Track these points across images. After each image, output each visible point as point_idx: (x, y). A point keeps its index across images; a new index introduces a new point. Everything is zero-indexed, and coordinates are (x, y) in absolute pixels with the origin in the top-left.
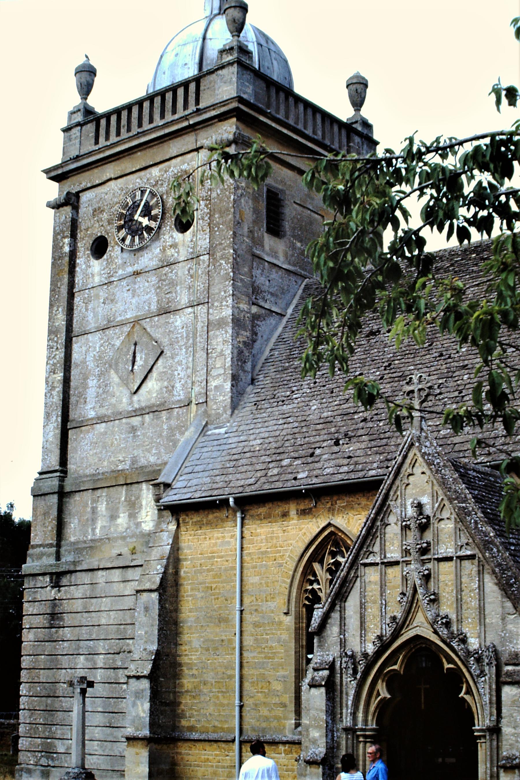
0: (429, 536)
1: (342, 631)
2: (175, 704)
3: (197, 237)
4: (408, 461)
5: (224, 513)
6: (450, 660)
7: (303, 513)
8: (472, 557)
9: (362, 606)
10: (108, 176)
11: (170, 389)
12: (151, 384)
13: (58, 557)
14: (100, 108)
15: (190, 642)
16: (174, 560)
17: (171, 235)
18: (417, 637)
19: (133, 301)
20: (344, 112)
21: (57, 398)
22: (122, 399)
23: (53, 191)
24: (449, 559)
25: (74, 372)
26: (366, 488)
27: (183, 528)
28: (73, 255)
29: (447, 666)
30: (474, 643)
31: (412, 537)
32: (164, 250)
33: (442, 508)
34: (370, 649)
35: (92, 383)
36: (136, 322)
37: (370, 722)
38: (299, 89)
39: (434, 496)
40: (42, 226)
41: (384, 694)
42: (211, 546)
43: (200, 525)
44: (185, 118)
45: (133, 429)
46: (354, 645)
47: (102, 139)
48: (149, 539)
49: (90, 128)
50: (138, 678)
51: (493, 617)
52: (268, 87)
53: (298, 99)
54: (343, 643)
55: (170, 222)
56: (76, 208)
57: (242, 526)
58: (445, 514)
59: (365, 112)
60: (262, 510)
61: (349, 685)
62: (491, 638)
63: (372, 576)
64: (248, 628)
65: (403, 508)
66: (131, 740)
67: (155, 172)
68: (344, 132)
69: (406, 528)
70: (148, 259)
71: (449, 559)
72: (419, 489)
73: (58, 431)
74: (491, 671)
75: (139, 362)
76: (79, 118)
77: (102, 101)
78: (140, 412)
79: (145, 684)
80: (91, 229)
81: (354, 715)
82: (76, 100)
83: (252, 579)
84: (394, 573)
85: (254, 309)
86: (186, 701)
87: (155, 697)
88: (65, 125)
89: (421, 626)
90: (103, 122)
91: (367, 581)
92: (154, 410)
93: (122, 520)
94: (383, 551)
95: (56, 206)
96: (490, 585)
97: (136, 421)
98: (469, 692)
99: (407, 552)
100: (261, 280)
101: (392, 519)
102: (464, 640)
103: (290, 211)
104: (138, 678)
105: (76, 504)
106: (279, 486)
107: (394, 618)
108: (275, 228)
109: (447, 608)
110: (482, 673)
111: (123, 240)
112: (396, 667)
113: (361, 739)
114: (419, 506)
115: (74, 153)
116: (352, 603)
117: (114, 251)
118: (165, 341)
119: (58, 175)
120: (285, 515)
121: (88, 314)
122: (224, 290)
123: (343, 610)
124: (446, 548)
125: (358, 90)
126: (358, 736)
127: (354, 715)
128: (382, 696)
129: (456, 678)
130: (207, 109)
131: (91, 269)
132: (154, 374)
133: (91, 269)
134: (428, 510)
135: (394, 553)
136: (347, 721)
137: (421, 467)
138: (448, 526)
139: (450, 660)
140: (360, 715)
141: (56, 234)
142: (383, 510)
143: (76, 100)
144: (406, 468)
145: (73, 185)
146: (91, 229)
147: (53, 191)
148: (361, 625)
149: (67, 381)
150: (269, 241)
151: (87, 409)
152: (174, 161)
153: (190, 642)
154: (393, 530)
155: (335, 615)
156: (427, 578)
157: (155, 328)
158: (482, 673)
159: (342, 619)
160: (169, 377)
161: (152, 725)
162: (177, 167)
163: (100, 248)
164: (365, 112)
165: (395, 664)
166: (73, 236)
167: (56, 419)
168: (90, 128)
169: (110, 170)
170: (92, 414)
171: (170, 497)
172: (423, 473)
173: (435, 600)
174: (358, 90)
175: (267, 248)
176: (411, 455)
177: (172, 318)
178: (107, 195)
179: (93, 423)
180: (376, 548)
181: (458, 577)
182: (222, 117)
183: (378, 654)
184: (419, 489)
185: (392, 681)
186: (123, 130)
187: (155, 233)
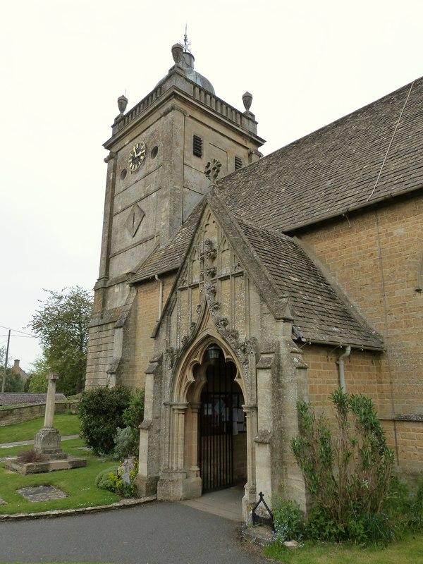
1: (169, 336)
4: (205, 215)
5: (154, 285)
8: (241, 274)
15: (300, 374)
18: (208, 336)
19: (135, 192)
20: (242, 109)
21: (105, 245)
23: (107, 153)
27: (139, 295)
28: (114, 179)
29: (226, 357)
30: (242, 338)
31: (208, 262)
37: (181, 399)
53: (218, 100)
54: (168, 343)
55: (149, 154)
57: (163, 289)
59: (251, 110)
61: (168, 372)
62: (256, 333)
69: (203, 259)
71: (226, 278)
74: (252, 358)
89: (210, 329)
91: (182, 300)
95: (106, 161)
98: (239, 377)
102: (235, 336)
103: (206, 148)
110: (246, 362)
112: (196, 359)
113: (176, 412)
114: (210, 243)
116: (174, 319)
118: (145, 210)
119: (108, 146)
123: (169, 321)
124: (225, 271)
125: (247, 99)
126: (174, 409)
128: (189, 380)
129: (231, 369)
131: (120, 184)
134: (216, 246)
135: (196, 280)
136: (167, 399)
137: (213, 218)
138: (227, 256)
139: (228, 354)
140: (175, 395)
141: (108, 172)
145: (114, 150)
147: (107, 153)
149: (109, 237)
150: (195, 159)
153: (300, 374)
155: (164, 325)
156: (214, 292)
157: (142, 205)
159: (169, 327)
162: (152, 129)
164: (251, 110)
165: (196, 357)
172: (214, 222)
173: (217, 307)
174: (247, 99)
175: (194, 162)
176: (206, 211)
179: (119, 253)
185: (196, 369)
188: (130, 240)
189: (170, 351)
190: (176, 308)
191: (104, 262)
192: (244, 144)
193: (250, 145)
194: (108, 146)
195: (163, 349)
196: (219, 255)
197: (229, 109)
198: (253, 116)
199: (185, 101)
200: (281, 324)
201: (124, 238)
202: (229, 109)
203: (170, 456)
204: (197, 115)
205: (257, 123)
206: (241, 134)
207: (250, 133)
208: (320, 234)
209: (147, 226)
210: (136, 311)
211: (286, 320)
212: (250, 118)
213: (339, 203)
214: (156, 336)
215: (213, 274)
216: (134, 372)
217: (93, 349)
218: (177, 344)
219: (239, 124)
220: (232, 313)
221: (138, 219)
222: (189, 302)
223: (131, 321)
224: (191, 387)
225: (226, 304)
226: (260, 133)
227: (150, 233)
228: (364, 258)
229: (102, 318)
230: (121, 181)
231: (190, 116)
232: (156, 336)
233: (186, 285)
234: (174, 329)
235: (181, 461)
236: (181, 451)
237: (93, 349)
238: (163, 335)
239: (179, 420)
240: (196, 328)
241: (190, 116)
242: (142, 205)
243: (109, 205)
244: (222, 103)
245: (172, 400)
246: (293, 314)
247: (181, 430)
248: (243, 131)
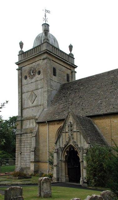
0: (72, 128)
1: (59, 143)
2: (38, 156)
3: (41, 76)
5: (45, 124)
6: (76, 149)
7: (58, 124)
8: (79, 131)
9: (62, 139)
10: (27, 64)
11: (38, 103)
12: (35, 102)
13: (21, 131)
14: (25, 51)
16: (38, 132)
17: (37, 76)
19: (32, 87)
20: (68, 52)
21: (20, 104)
22: (31, 104)
23: (17, 67)
24: (75, 132)
25: (23, 100)
26: (63, 120)
28: (21, 79)
30: (79, 146)
31: (70, 127)
32: (36, 78)
33: (74, 123)
34: (64, 146)
35: (26, 101)
36: (32, 91)
38: (60, 49)
39: (73, 121)
40: (15, 74)
41: (66, 154)
42: (44, 129)
43: (42, 126)
44: (38, 53)
45: (33, 110)
46: (61, 146)
47: (25, 57)
48: (33, 129)
49: (23, 55)
50: (32, 151)
51: (82, 142)
52: (53, 47)
53: (61, 51)
54: (60, 145)
55: (37, 73)
56: (21, 70)
58: (75, 124)
59: (72, 52)
60: (51, 123)
62: (82, 145)
63: (64, 134)
64: (50, 143)
65: (68, 123)
66: (31, 162)
67: (34, 64)
68: (68, 56)
69: (69, 126)
70: (33, 80)
71: (75, 132)
72: (71, 120)
73: (21, 110)
74: (82, 151)
75: (33, 98)
76: (21, 53)
77: (25, 49)
78: (33, 107)
79: (33, 153)
80: (25, 74)
81: (61, 158)
82: (20, 49)
83: (50, 135)
84: (67, 134)
85: (51, 89)
86: (40, 155)
87: (35, 154)
88: (18, 54)
89: (71, 143)
90: (25, 54)
92: (35, 106)
93: (31, 125)
94: (65, 130)
96: (82, 137)
97: (33, 108)
98: (79, 155)
99: (69, 130)
100: (52, 84)
101: (67, 125)
102: (78, 146)
103: (57, 72)
104: (32, 151)
105: (25, 122)
106: (54, 119)
107: (67, 141)
108: (55, 75)
109: (75, 140)
110: (80, 151)
111: (29, 76)
114: (71, 123)
115: (21, 60)
117: (28, 78)
118: (37, 94)
119: (18, 64)
120: (55, 124)
121: (25, 89)
122: (45, 85)
124: (75, 130)
125: (71, 47)
127: (61, 158)
129: (77, 153)
130: (42, 51)
131: (24, 81)
132: (35, 100)
133: (24, 81)
134: (72, 123)
135: (67, 131)
136: (60, 159)
137: (71, 116)
138: (75, 126)
139: (76, 149)
142: (65, 123)
143: (20, 49)
144: (69, 116)
145: (21, 66)
146: (25, 74)
147: (17, 67)
148: (63, 143)
149: (22, 101)
150: (54, 77)
151: (25, 106)
152: (37, 62)
154: (67, 127)
155: (58, 141)
156: (72, 135)
157: (36, 92)
158: (80, 151)
159: (59, 142)
160: (38, 101)
161: (34, 159)
162: (37, 63)
163: (26, 78)
164: (72, 52)
166: (21, 76)
167: (20, 108)
168: (23, 55)
169: (26, 63)
170: (26, 107)
171: (37, 121)
173: (73, 139)
174: (71, 47)
175: (53, 78)
176: (69, 114)
177: (38, 90)
178: (27, 68)
180: (64, 130)
181: (77, 135)
182: (44, 53)
183: (65, 147)
184: (71, 120)
185: (67, 152)
186: (27, 56)
187: (34, 75)
188: (31, 104)
189: (60, 148)
190: (61, 137)
191: (20, 111)
192: (70, 68)
193: (72, 69)
194: (18, 64)
195: (58, 147)
196: (73, 126)
197: (63, 53)
198: (73, 55)
199: (50, 54)
200: (88, 144)
201: (28, 103)
202: (63, 53)
203: (62, 172)
204: (54, 59)
205: (75, 67)
206: (69, 65)
207: (72, 64)
208: (96, 118)
209: (38, 101)
210: (39, 132)
211: (89, 143)
212: (71, 56)
213: (102, 110)
214: (56, 143)
215: (72, 130)
216: (39, 151)
217: (18, 142)
218: (62, 146)
219: (67, 61)
220: (77, 140)
221: (33, 98)
222: (65, 136)
223: (37, 135)
224: (66, 156)
225: (75, 138)
226: (74, 57)
227: (39, 104)
228: (107, 126)
229: (21, 131)
230: (25, 80)
231: (52, 60)
232: (56, 143)
233: (64, 131)
234: (61, 142)
235: (64, 173)
236: (64, 171)
237: (18, 142)
238: (58, 143)
239: (63, 164)
240: (68, 143)
241: (52, 60)
242: (36, 92)
243: (20, 90)
244: (62, 52)
245: (61, 159)
246: (91, 142)
247: (64, 166)
248: (70, 64)
